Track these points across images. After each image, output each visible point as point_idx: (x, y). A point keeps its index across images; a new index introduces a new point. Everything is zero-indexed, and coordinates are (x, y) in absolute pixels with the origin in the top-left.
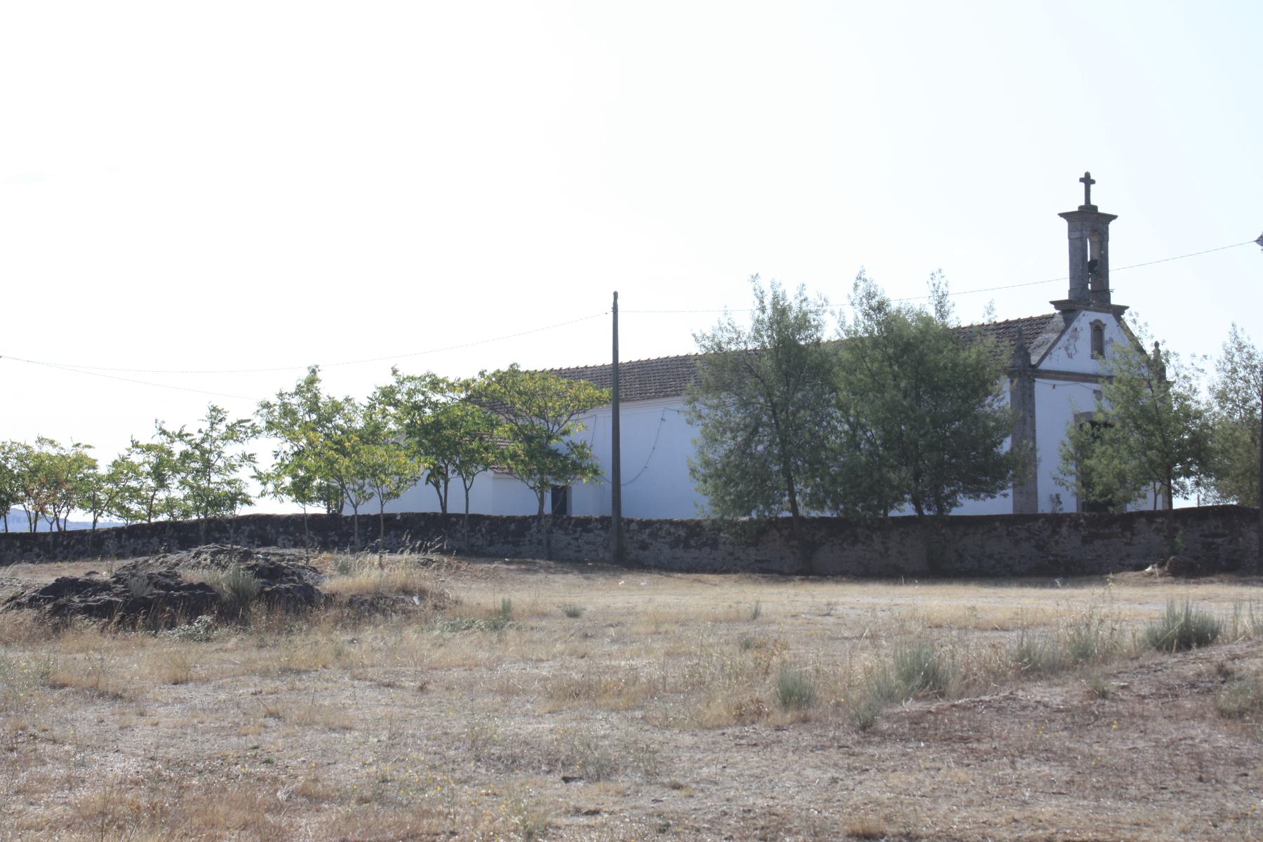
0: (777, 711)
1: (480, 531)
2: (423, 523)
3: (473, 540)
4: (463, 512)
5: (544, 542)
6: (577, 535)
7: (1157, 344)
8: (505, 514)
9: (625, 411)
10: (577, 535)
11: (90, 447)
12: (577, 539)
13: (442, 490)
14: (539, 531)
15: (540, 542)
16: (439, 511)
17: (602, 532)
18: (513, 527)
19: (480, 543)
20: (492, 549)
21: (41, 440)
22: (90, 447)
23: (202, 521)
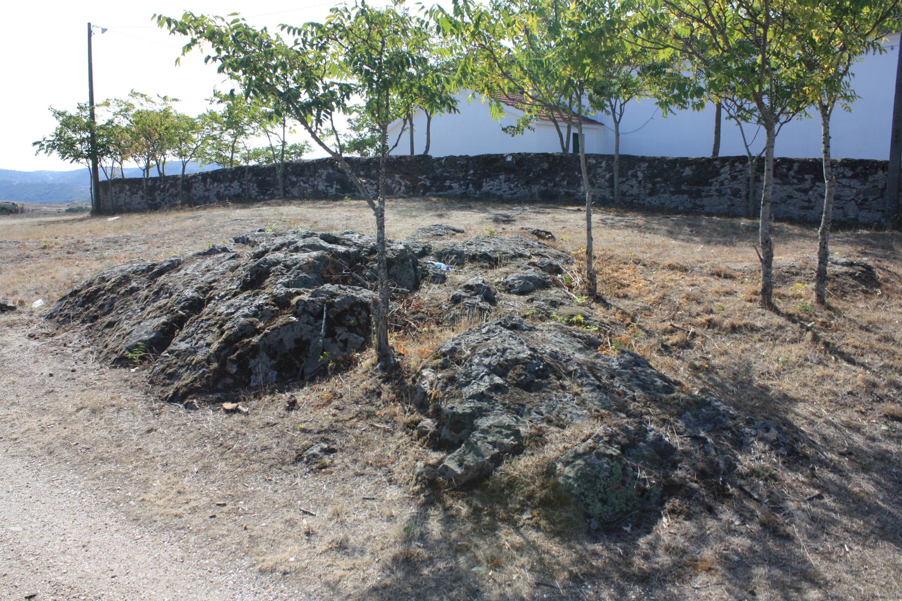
0: (164, 107)
1: (635, 176)
2: (545, 166)
3: (625, 187)
4: (819, 154)
5: (743, 193)
6: (807, 185)
7: (501, 111)
8: (857, 158)
9: (434, 116)
10: (807, 185)
11: (176, 100)
12: (805, 191)
13: (618, 117)
14: (734, 178)
15: (736, 193)
16: (409, 154)
17: (855, 183)
18: (688, 171)
19: (635, 191)
20: (654, 201)
21: (134, 94)
22: (176, 100)
23: (279, 165)
